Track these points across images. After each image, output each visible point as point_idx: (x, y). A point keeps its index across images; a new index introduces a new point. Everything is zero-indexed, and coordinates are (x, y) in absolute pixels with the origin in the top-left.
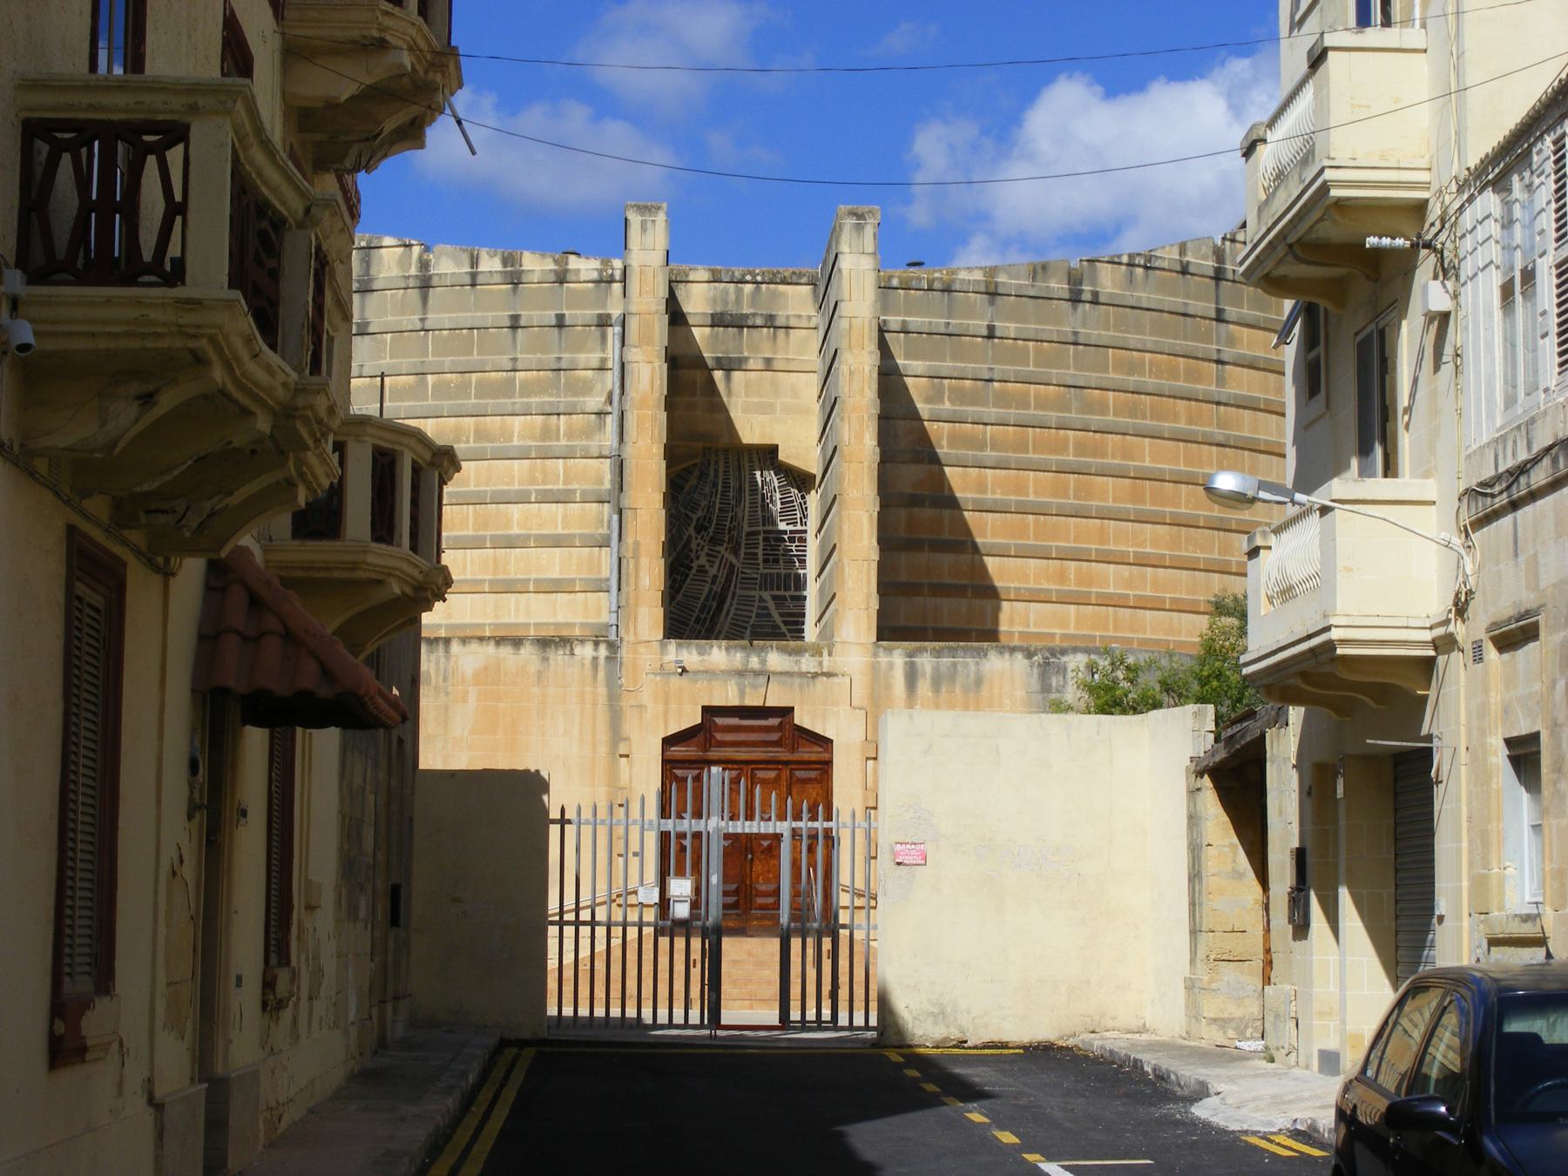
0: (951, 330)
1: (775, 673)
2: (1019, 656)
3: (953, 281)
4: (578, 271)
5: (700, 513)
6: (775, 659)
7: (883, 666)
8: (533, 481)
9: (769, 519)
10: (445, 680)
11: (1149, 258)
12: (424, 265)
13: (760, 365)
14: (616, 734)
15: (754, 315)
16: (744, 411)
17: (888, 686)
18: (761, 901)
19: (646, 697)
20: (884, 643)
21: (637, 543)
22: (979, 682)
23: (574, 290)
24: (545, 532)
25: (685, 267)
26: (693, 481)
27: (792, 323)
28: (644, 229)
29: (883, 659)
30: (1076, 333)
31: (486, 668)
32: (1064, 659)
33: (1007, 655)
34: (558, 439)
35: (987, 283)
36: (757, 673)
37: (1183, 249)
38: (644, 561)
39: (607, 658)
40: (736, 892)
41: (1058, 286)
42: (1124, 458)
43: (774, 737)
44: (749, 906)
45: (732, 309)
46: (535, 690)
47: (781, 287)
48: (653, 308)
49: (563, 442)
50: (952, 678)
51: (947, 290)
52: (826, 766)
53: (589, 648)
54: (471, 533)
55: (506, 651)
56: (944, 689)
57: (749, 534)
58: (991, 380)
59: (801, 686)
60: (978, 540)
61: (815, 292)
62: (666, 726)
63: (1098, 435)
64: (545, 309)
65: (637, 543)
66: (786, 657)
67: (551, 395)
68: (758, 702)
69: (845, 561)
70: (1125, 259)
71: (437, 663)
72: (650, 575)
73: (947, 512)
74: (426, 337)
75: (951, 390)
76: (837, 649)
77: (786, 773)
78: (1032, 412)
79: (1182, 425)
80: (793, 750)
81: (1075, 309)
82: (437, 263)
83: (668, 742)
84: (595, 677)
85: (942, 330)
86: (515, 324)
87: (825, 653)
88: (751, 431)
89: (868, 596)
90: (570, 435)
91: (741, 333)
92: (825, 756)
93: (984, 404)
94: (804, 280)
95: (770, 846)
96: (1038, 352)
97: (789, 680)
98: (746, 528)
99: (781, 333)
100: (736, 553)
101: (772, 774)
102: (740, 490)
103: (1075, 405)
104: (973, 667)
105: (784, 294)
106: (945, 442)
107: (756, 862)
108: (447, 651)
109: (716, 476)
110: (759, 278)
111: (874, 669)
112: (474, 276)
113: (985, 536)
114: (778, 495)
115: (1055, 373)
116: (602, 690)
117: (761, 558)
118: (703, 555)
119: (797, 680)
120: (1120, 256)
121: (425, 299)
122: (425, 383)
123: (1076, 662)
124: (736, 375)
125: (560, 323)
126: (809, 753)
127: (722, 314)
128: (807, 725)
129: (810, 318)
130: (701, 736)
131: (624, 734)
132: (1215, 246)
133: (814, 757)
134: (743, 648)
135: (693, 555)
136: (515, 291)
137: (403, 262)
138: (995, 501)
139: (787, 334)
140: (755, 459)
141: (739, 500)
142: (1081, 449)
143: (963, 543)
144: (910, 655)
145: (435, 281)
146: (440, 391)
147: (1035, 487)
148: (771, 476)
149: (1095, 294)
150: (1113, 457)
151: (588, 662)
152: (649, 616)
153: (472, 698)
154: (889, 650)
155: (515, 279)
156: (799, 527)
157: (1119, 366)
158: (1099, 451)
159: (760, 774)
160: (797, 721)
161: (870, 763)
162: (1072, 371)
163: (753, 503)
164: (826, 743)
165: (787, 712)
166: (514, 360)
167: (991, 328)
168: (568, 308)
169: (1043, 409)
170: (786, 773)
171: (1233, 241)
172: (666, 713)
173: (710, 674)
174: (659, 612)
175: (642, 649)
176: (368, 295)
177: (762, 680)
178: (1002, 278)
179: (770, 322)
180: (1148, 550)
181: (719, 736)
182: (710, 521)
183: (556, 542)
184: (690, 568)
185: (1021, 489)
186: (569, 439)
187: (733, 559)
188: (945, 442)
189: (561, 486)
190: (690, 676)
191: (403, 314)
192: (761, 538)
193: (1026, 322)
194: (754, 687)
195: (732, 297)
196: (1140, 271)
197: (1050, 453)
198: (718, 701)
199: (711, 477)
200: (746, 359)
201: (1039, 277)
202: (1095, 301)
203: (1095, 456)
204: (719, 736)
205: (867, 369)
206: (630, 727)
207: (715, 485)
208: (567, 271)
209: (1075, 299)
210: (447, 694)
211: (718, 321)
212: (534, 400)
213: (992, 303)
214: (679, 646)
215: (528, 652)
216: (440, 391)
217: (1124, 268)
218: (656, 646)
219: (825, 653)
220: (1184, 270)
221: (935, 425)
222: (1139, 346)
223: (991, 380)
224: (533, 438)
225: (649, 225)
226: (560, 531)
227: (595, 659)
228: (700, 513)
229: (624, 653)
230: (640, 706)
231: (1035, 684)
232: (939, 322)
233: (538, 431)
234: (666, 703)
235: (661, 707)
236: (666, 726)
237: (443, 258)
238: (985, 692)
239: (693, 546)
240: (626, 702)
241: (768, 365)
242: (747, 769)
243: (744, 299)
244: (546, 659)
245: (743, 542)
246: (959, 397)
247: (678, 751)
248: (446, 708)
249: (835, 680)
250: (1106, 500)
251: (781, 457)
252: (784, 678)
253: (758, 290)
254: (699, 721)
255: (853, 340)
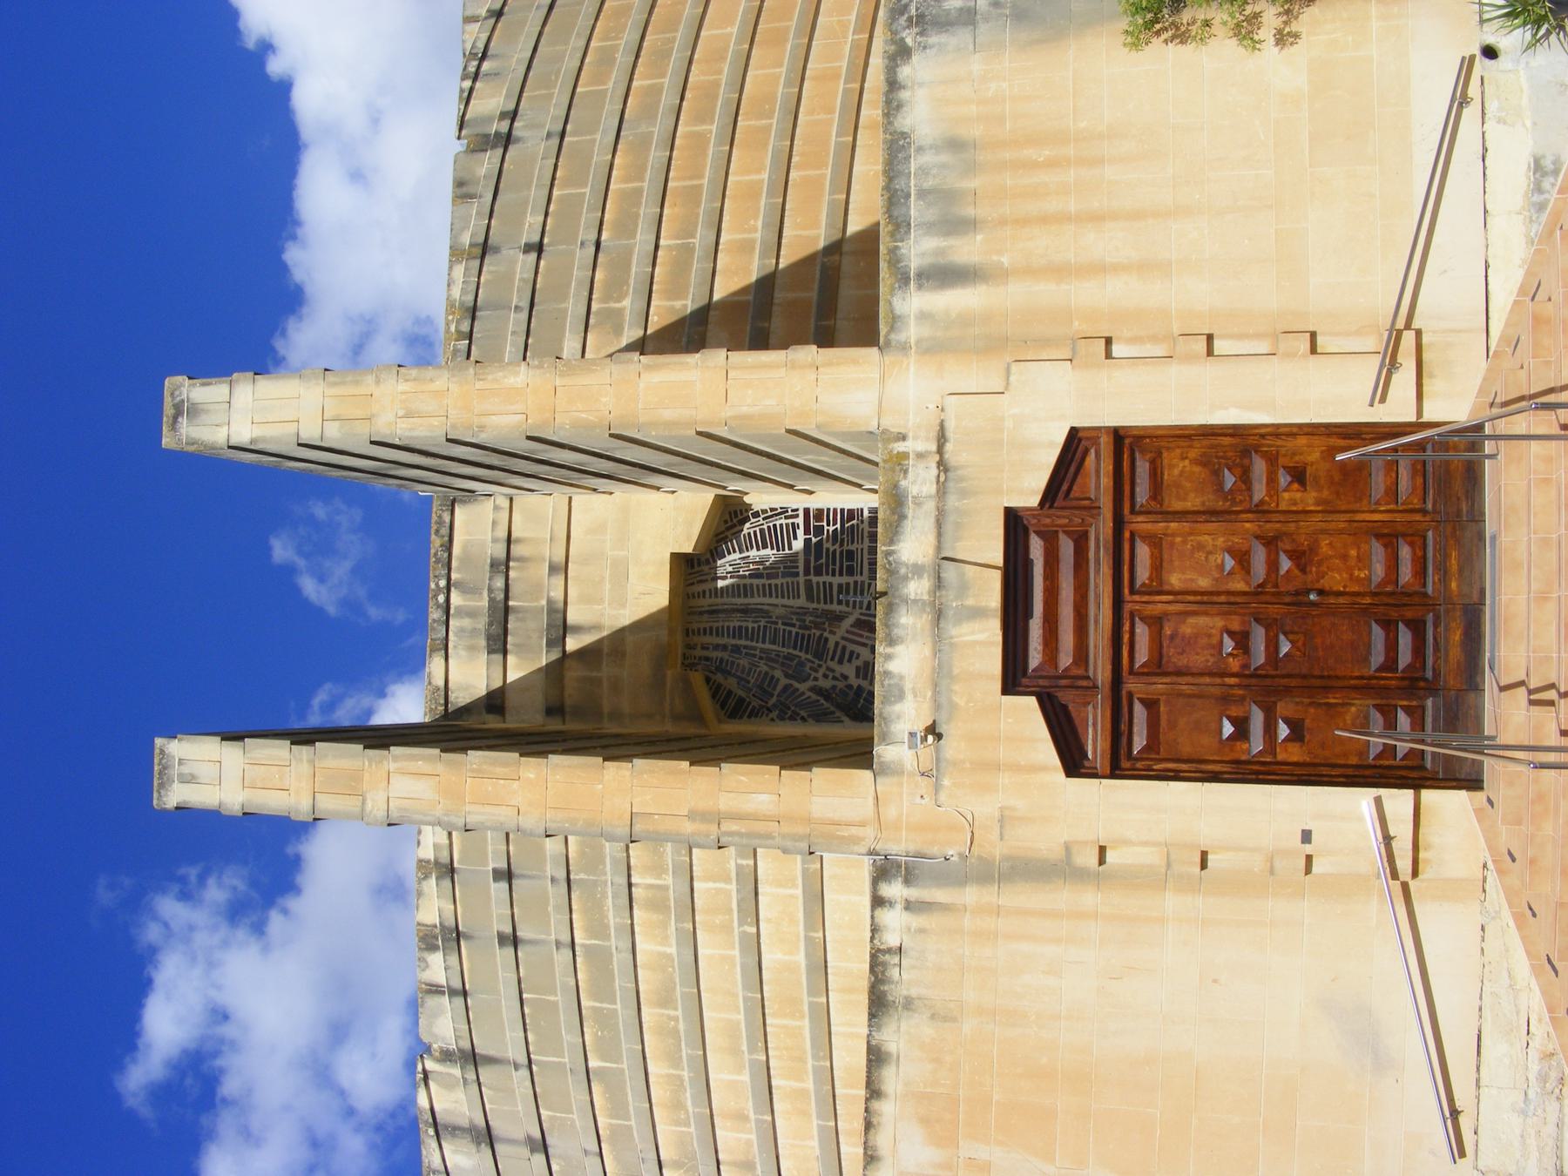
0: (525, 304)
1: (939, 548)
2: (905, 72)
3: (462, 304)
5: (778, 674)
6: (912, 546)
7: (926, 331)
8: (727, 929)
9: (788, 565)
11: (473, 55)
12: (447, 1056)
15: (490, 590)
16: (623, 606)
17: (965, 320)
18: (1406, 574)
19: (984, 808)
20: (883, 329)
21: (692, 816)
22: (955, 145)
23: (462, 852)
24: (801, 915)
25: (366, 701)
26: (731, 683)
28: (190, 779)
29: (912, 332)
30: (549, 135)
31: (925, 1121)
33: (904, 95)
34: (665, 888)
36: (939, 583)
38: (726, 802)
39: (907, 882)
41: (487, 162)
42: (723, 59)
43: (1067, 547)
44: (1417, 597)
45: (482, 623)
46: (968, 1027)
47: (457, 549)
48: (305, 768)
49: (669, 880)
50: (946, 196)
51: (473, 312)
52: (1123, 441)
53: (889, 917)
54: (807, 1021)
55: (890, 1079)
57: (810, 598)
58: (598, 245)
59: (964, 494)
60: (821, 244)
61: (463, 502)
62: (1043, 768)
63: (688, 95)
65: (692, 816)
66: (908, 525)
67: (604, 895)
68: (995, 581)
69: (728, 413)
72: (749, 790)
73: (779, 296)
74: (539, 1063)
75: (607, 298)
76: (891, 423)
77: (1141, 524)
78: (646, 185)
80: (1093, 509)
81: (518, 140)
82: (443, 1039)
83: (1074, 763)
84: (944, 908)
85: (525, 315)
86: (512, 940)
87: (900, 447)
88: (648, 593)
89: (793, 366)
90: (658, 869)
91: (517, 610)
92: (1106, 442)
95: (1295, 555)
96: (567, 183)
97: (951, 519)
98: (802, 601)
99: (516, 550)
100: (840, 618)
101: (1143, 552)
102: (745, 611)
103: (643, 128)
104: (927, 159)
105: (465, 547)
106: (678, 304)
107: (1325, 583)
109: (724, 647)
110: (443, 583)
111: (932, 349)
112: (453, 993)
113: (817, 238)
114: (753, 553)
115: (600, 157)
116: (970, 895)
117: (845, 579)
118: (839, 669)
119: (952, 501)
120: (462, 91)
121: (491, 1060)
122: (601, 1071)
124: (572, 618)
126: (1098, 476)
127: (489, 638)
128: (1040, 480)
129: (496, 508)
130: (1066, 697)
131: (1057, 853)
133: (1107, 466)
134: (890, 609)
135: (840, 685)
136: (468, 937)
137: (449, 1085)
138: (766, 225)
139: (519, 541)
140: (699, 588)
142: (703, 117)
143: (825, 269)
144: (904, 280)
145: (466, 1045)
147: (751, 172)
149: (503, 115)
150: (720, 72)
151: (916, 921)
152: (829, 793)
153: (982, 1152)
154: (895, 320)
156: (800, 521)
157: (600, 78)
158: (710, 92)
159: (1143, 574)
160: (1033, 501)
162: (598, 137)
163: (767, 591)
164: (1076, 444)
165: (1014, 521)
166: (558, 944)
167: (528, 248)
168: (486, 865)
169: (643, 169)
170: (1141, 524)
172: (1017, 768)
173: (940, 676)
174: (823, 777)
175: (890, 812)
176: (495, 1132)
177: (950, 572)
178: (466, 239)
179: (502, 566)
180: (853, 18)
181: (1065, 660)
182: (789, 657)
183: (816, 899)
185: (752, 192)
186: (665, 871)
188: (678, 304)
189: (733, 887)
192: (815, 579)
193: (527, 202)
194: (964, 588)
195: (467, 622)
196: (486, 66)
199: (725, 655)
202: (513, 115)
203: (716, 97)
204: (1065, 660)
206: (1043, 841)
207: (736, 649)
208: (437, 863)
209: (507, 140)
212: (612, 919)
213: (497, 250)
214: (885, 738)
215: (893, 1037)
219: (900, 447)
221: (653, 318)
222: (579, 55)
223: (598, 245)
224: (665, 925)
225: (186, 770)
226: (799, 891)
227: (909, 906)
228: (778, 674)
229: (898, 847)
232: (516, 320)
233: (655, 917)
235: (1004, 779)
236: (1043, 768)
237: (436, 1030)
238: (975, 132)
239: (826, 684)
240: (994, 847)
241: (561, 568)
242: (1131, 603)
243: (469, 606)
244: (908, 1004)
245: (822, 606)
246: (616, 288)
247: (1095, 744)
249: (951, 426)
251: (688, 548)
252: (948, 528)
253: (461, 586)
255: (359, 413)
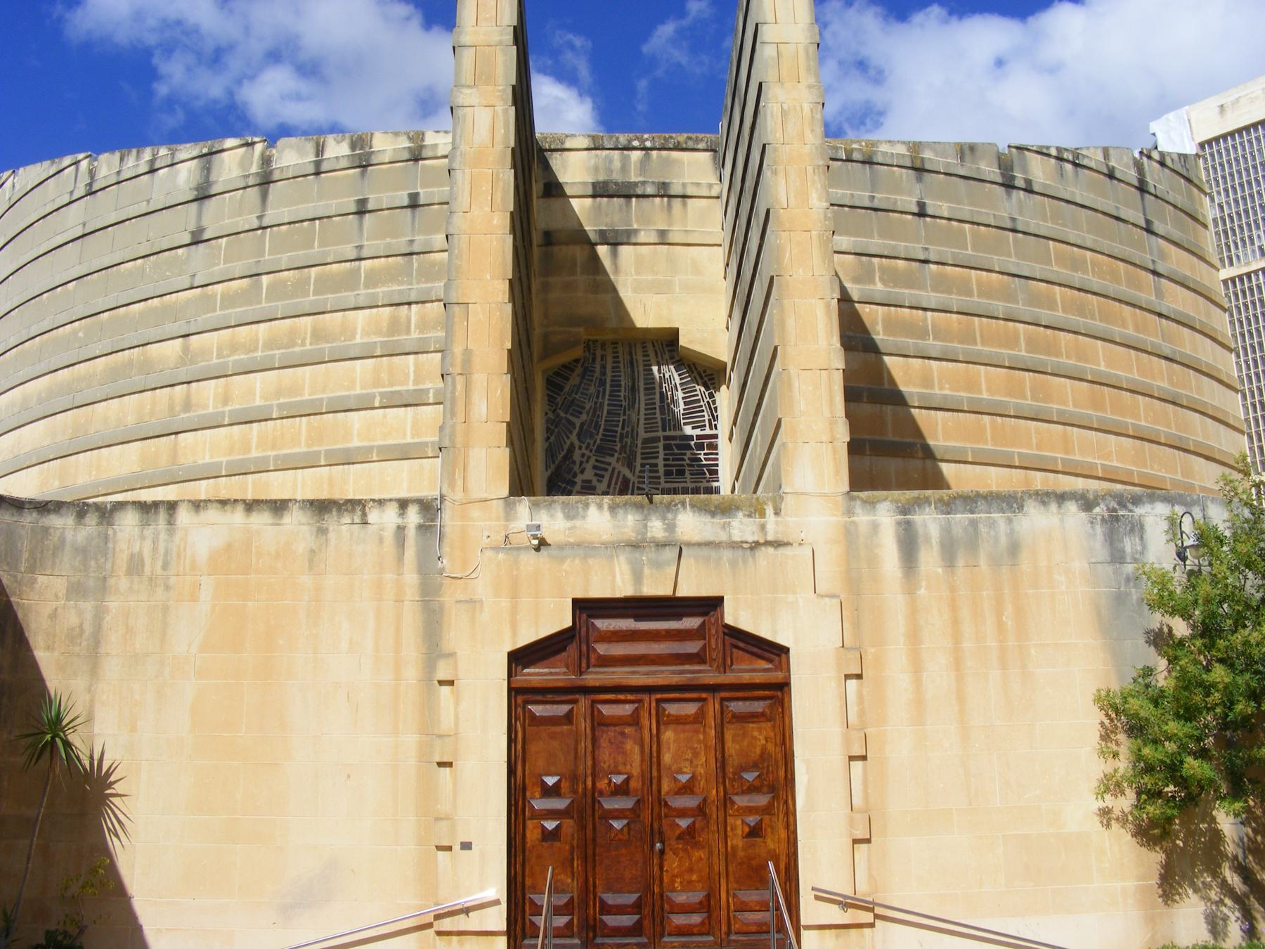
0: (876, 204)
1: (689, 544)
2: (1072, 507)
4: (435, 146)
5: (584, 417)
6: (690, 523)
7: (863, 529)
9: (672, 422)
10: (165, 566)
11: (1077, 156)
12: (266, 161)
13: (653, 238)
14: (433, 645)
15: (644, 183)
16: (635, 290)
17: (873, 561)
18: (679, 920)
19: (482, 587)
21: (468, 353)
22: (1014, 549)
23: (432, 167)
24: (390, 442)
26: (575, 379)
27: (689, 192)
29: (862, 518)
30: (1013, 220)
31: (229, 547)
32: (1139, 511)
33: (1053, 507)
34: (408, 332)
35: (913, 159)
36: (660, 545)
37: (1106, 152)
38: (479, 379)
39: (420, 527)
40: (919, 506)
41: (990, 170)
43: (692, 647)
45: (617, 177)
46: (306, 580)
47: (675, 154)
48: (496, 38)
49: (415, 335)
50: (973, 542)
51: (868, 162)
52: (778, 692)
55: (261, 519)
56: (960, 562)
57: (646, 441)
58: (926, 262)
59: (734, 564)
60: (931, 442)
61: (715, 158)
62: (514, 633)
63: (1049, 331)
64: (396, 190)
65: (468, 353)
66: (707, 519)
69: (793, 371)
70: (1054, 152)
71: (155, 542)
72: (489, 397)
73: (889, 409)
74: (263, 235)
75: (881, 268)
76: (788, 503)
77: (713, 706)
78: (976, 299)
79: (1130, 331)
80: (724, 668)
81: (1009, 195)
83: (519, 658)
84: (400, 558)
85: (867, 204)
87: (769, 511)
88: (646, 310)
89: (832, 422)
91: (629, 205)
92: (778, 676)
93: (922, 287)
94: (701, 146)
95: (691, 830)
97: (713, 553)
99: (677, 203)
100: (630, 466)
101: (690, 709)
102: (634, 389)
103: (1020, 296)
104: (1002, 526)
106: (880, 328)
107: (669, 855)
108: (171, 522)
109: (604, 374)
110: (648, 144)
111: (849, 534)
112: (318, 164)
113: (936, 439)
114: (680, 394)
115: (996, 261)
116: (411, 578)
117: (661, 469)
118: (589, 467)
119: (727, 554)
120: (1048, 148)
121: (264, 197)
123: (1154, 516)
124: (624, 250)
125: (414, 203)
126: (751, 671)
127: (605, 183)
129: (710, 186)
130: (572, 650)
132: (1135, 159)
133: (759, 678)
134: (639, 507)
135: (576, 468)
136: (363, 174)
137: (243, 163)
138: (945, 397)
139: (685, 205)
141: (633, 401)
142: (1032, 344)
143: (911, 445)
144: (904, 511)
145: (276, 176)
146: (276, 292)
147: (988, 384)
148: (671, 372)
149: (1028, 182)
152: (489, 461)
153: (206, 595)
154: (872, 504)
155: (363, 163)
156: (708, 431)
157: (1061, 259)
159: (672, 709)
160: (729, 620)
161: (852, 684)
163: (650, 406)
164: (777, 653)
165: (712, 605)
167: (921, 205)
170: (713, 706)
171: (1149, 157)
172: (514, 611)
173: (585, 548)
174: (503, 456)
175: (475, 512)
179: (664, 192)
180: (1115, 464)
181: (602, 649)
182: (597, 426)
183: (404, 453)
184: (574, 483)
185: (972, 385)
186: (421, 332)
187: (626, 472)
188: (880, 328)
189: (411, 387)
190: (553, 551)
191: (240, 215)
192: (661, 445)
194: (657, 565)
195: (617, 165)
196: (1068, 167)
197: (1001, 346)
198: (598, 590)
199: (597, 374)
200: (636, 232)
201: (968, 158)
202: (1029, 190)
204: (602, 649)
205: (806, 108)
206: (456, 635)
207: (602, 383)
209: (1009, 185)
210: (167, 588)
211: (601, 191)
212: (381, 290)
213: (919, 180)
214: (535, 505)
216: (276, 292)
217: (1053, 161)
218: (498, 507)
219: (769, 511)
220: (1111, 175)
222: (1079, 242)
223: (926, 262)
226: (409, 440)
227: (401, 529)
230: (472, 601)
231: (1101, 552)
232: (862, 197)
234: (515, 595)
235: (505, 602)
236: (514, 633)
237: (287, 151)
238: (1025, 565)
239: (577, 456)
240: (450, 596)
241: (663, 239)
242: (649, 700)
243: (631, 166)
244: (322, 531)
245: (639, 451)
246: (891, 278)
247: (535, 675)
248: (166, 609)
249: (787, 551)
250: (1065, 403)
251: (683, 342)
252: (705, 552)
254: (568, 623)
255: (784, 72)
